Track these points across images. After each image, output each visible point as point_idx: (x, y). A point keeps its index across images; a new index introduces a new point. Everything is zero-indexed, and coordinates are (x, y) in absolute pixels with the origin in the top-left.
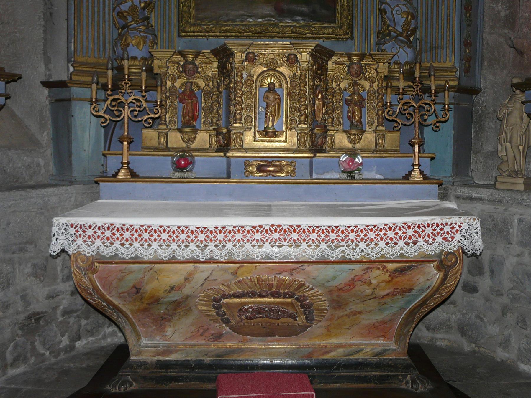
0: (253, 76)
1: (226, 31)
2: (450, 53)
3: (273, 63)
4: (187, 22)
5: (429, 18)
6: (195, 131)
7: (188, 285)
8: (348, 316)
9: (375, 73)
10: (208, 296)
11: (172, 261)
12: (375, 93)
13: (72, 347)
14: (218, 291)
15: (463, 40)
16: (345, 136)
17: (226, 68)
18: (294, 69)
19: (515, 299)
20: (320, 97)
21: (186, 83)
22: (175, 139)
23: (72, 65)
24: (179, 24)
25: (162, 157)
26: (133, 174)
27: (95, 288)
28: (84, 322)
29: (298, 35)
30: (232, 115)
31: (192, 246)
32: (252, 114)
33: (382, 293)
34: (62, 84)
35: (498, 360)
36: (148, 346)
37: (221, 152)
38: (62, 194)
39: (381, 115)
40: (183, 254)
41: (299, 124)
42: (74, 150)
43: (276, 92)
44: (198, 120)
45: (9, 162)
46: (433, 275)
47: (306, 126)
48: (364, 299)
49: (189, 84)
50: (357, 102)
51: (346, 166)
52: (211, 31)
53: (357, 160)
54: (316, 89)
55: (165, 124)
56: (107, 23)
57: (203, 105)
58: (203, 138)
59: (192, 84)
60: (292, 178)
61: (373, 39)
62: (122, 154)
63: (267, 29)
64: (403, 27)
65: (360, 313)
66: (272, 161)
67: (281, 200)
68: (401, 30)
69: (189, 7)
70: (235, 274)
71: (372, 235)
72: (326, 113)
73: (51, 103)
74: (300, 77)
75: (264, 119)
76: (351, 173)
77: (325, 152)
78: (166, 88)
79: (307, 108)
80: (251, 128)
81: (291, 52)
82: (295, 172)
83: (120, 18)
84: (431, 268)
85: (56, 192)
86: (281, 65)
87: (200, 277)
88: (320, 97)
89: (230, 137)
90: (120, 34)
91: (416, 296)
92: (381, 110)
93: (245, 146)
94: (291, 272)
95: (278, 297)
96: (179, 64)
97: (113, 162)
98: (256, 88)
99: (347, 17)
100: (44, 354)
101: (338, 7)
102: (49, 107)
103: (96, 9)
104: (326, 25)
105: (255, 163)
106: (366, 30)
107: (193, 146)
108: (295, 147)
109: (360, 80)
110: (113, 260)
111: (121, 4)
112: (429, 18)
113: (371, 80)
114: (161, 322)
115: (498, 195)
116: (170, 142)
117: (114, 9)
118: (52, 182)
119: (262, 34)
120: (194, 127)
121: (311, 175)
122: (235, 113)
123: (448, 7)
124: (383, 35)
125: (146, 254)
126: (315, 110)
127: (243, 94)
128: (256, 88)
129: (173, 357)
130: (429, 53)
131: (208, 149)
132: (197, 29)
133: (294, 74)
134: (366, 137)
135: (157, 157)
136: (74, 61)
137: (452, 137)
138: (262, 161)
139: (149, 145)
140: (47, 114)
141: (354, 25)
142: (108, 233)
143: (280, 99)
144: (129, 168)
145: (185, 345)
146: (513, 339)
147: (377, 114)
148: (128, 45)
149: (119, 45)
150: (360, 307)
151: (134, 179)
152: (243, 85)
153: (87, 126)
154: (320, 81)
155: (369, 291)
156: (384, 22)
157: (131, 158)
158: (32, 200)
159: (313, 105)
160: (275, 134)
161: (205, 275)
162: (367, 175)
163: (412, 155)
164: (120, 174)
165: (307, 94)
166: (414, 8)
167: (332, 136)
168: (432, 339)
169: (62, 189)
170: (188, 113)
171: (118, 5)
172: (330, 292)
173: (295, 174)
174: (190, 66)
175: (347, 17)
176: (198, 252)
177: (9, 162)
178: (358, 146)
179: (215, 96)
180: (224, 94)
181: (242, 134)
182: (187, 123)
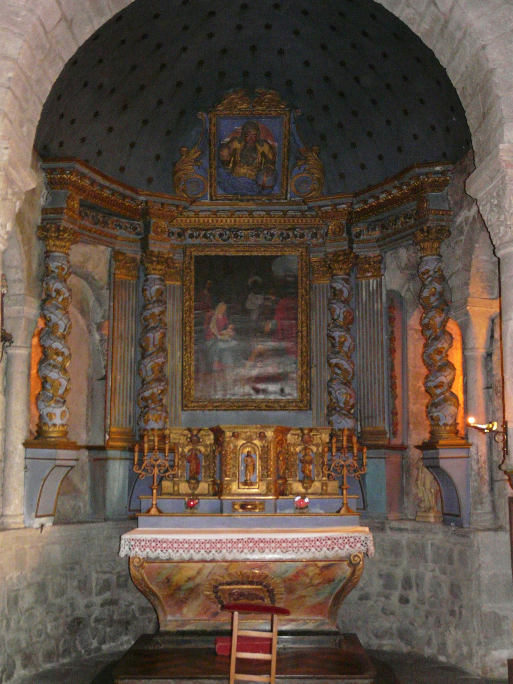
1: (217, 406)
6: (198, 482)
7: (199, 577)
8: (297, 599)
10: (210, 584)
11: (191, 561)
13: (99, 649)
14: (217, 580)
18: (264, 442)
19: (432, 605)
21: (192, 449)
22: (184, 488)
26: (160, 511)
27: (143, 579)
28: (108, 630)
31: (203, 552)
32: (237, 471)
33: (316, 582)
34: (102, 448)
35: (426, 656)
36: (171, 621)
40: (197, 557)
46: (346, 570)
48: (307, 586)
52: (205, 406)
58: (204, 487)
59: (196, 449)
61: (326, 411)
65: (304, 597)
70: (227, 569)
71: (307, 544)
75: (244, 474)
76: (302, 509)
77: (286, 495)
84: (345, 564)
86: (255, 439)
87: (206, 572)
89: (222, 486)
90: (142, 412)
91: (338, 584)
93: (163, 492)
94: (260, 568)
95: (253, 585)
100: (80, 652)
105: (239, 503)
107: (196, 492)
108: (264, 493)
110: (157, 559)
113: (317, 445)
114: (181, 603)
115: (417, 525)
118: (89, 520)
125: (175, 556)
129: (187, 628)
132: (196, 404)
140: (87, 469)
142: (154, 544)
144: (157, 507)
145: (195, 620)
146: (433, 638)
150: (304, 593)
155: (308, 581)
156: (331, 400)
157: (158, 501)
160: (251, 484)
161: (209, 570)
162: (313, 510)
167: (291, 484)
168: (380, 645)
172: (284, 581)
174: (195, 438)
175: (306, 395)
176: (206, 555)
178: (310, 491)
180: (218, 458)
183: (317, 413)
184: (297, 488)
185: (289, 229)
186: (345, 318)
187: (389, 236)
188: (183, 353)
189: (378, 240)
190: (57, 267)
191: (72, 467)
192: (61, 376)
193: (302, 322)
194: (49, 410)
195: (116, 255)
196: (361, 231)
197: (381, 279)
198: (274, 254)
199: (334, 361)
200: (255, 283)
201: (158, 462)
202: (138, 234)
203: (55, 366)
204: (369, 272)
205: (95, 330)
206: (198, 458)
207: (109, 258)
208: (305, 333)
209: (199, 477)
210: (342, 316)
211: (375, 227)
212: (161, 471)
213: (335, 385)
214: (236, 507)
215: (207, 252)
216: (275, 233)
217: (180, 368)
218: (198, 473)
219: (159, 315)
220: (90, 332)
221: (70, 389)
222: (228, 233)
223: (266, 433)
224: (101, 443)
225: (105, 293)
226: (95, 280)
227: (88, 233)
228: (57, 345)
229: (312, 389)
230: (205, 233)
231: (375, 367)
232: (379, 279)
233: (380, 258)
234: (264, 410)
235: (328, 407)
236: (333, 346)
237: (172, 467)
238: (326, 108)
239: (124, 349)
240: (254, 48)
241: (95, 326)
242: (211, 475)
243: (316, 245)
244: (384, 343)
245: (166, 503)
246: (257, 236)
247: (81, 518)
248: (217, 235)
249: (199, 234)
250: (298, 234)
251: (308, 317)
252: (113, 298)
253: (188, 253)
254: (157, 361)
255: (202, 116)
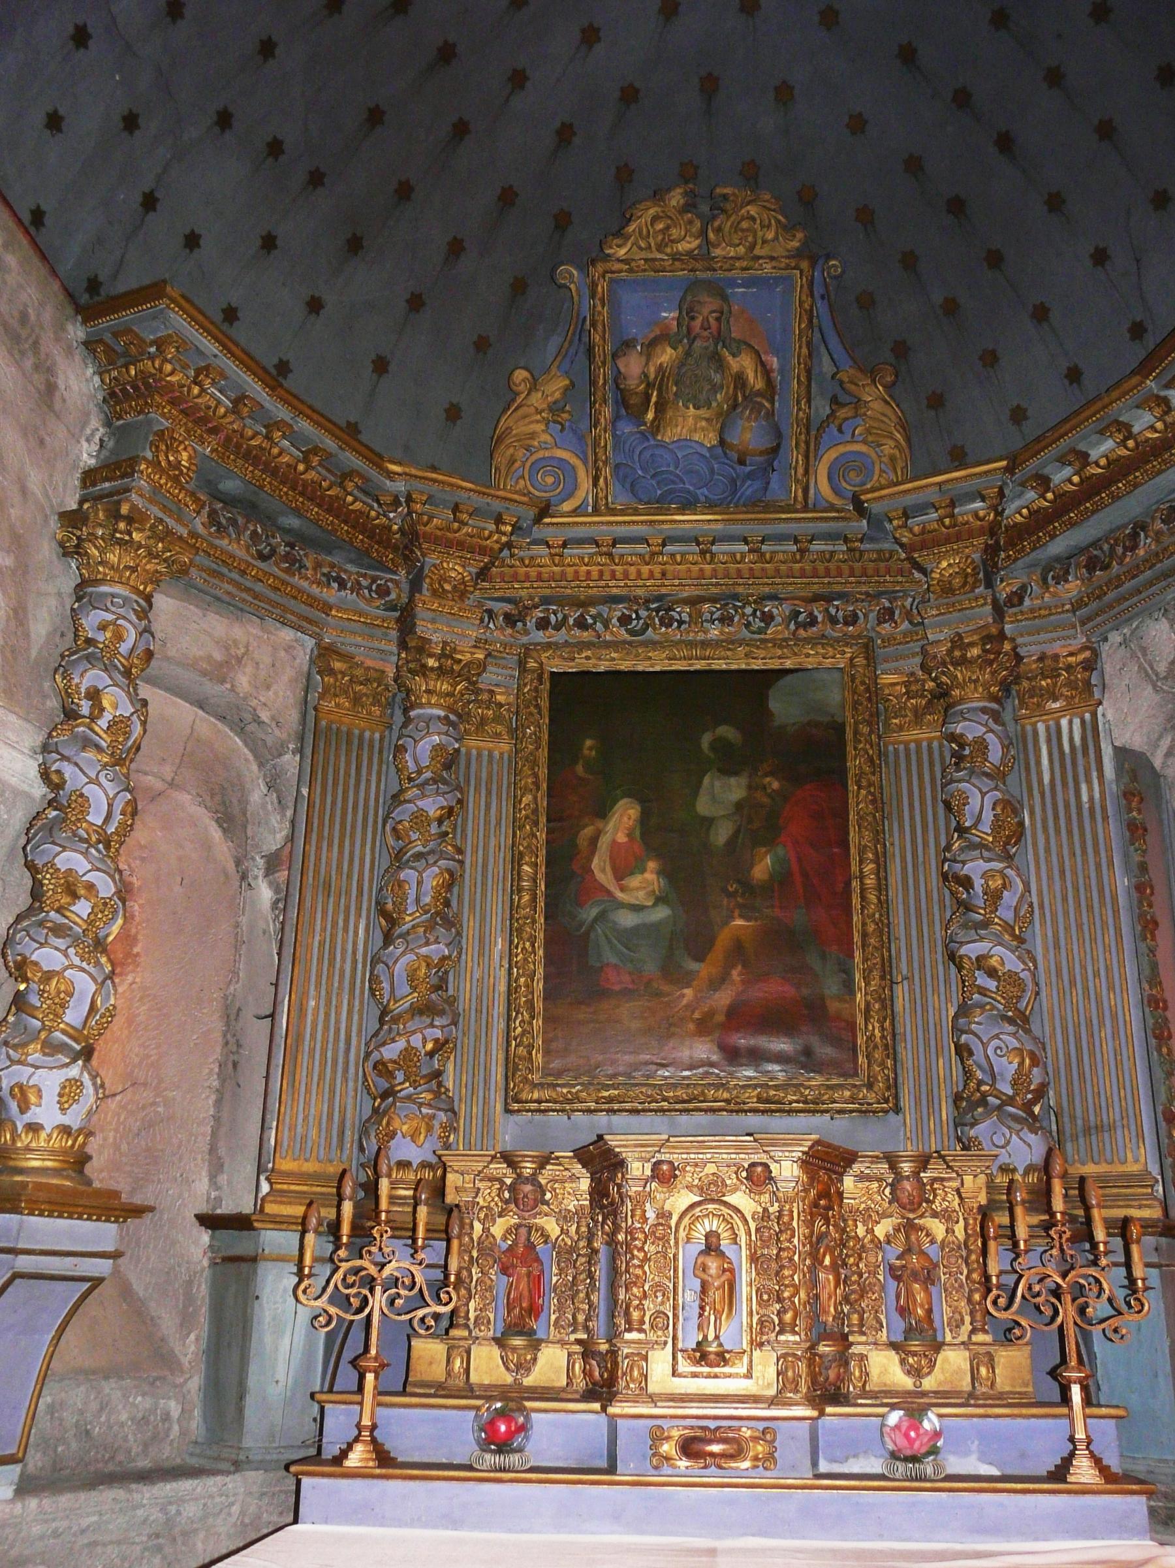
0: (671, 1214)
1: (610, 1100)
2: (1134, 1140)
3: (715, 1183)
4: (525, 1080)
5: (1074, 1059)
6: (535, 1345)
9: (957, 1200)
12: (959, 1248)
15: (1160, 1109)
16: (893, 1357)
17: (607, 1195)
18: (765, 1198)
20: (827, 1261)
21: (518, 1227)
22: (487, 1365)
23: (267, 1179)
24: (507, 1084)
25: (454, 1412)
29: (773, 1106)
30: (620, 1311)
34: (241, 1223)
37: (595, 1400)
38: (211, 1497)
39: (979, 1303)
41: (781, 1332)
42: (252, 1381)
43: (723, 1254)
44: (543, 1316)
45: (102, 1409)
47: (797, 1338)
49: (523, 1231)
50: (915, 1271)
51: (902, 1442)
53: (926, 1425)
54: (818, 1242)
55: (467, 1326)
56: (351, 1084)
57: (555, 1279)
58: (552, 1363)
59: (530, 1228)
60: (768, 1474)
61: (946, 1111)
62: (361, 1403)
63: (703, 1093)
64: (1015, 1083)
66: (718, 1428)
67: (745, 1534)
68: (1010, 1092)
69: (530, 1047)
72: (846, 1299)
73: (213, 1264)
74: (779, 1218)
75: (695, 1321)
76: (913, 1465)
78: (472, 1239)
79: (798, 1292)
80: (665, 1343)
81: (755, 1158)
82: (774, 1458)
83: (380, 1075)
85: (199, 1489)
86: (735, 1190)
88: (827, 1261)
89: (615, 1364)
90: (375, 1111)
92: (977, 1290)
96: (502, 1183)
97: (339, 1422)
98: (677, 1243)
99: (882, 1064)
101: (860, 1040)
102: (206, 1273)
103: (329, 1054)
104: (834, 1082)
105: (676, 1433)
106: (930, 1093)
108: (773, 1392)
109: (922, 1216)
111: (384, 1044)
112: (1074, 1059)
113: (946, 1216)
116: (476, 1370)
117: (368, 1055)
118: (194, 1462)
119: (691, 1106)
120: (531, 1333)
121: (815, 1464)
122: (628, 1307)
123: (1115, 1034)
124: (969, 1103)
126: (817, 1296)
127: (646, 1259)
128: (677, 1243)
130: (1081, 1140)
131: (563, 1390)
133: (765, 1210)
134: (946, 1360)
135: (443, 1412)
136: (273, 1170)
137: (1167, 1351)
138: (692, 1428)
139: (426, 1378)
140: (203, 1290)
141: (900, 1080)
143: (732, 1271)
144: (374, 1441)
147: (970, 1301)
148: (392, 1135)
149: (373, 1134)
151: (384, 1471)
152: (646, 1237)
153: (287, 1325)
154: (827, 1223)
156: (968, 1074)
157: (381, 1411)
158: (140, 1512)
159: (814, 1283)
160: (722, 1358)
162: (955, 1464)
163: (1065, 1410)
164: (351, 1455)
165: (796, 1258)
166: (1035, 1038)
167: (863, 1358)
169: (211, 1484)
170: (520, 1298)
171: (377, 1048)
173: (775, 1464)
174: (528, 1188)
175: (882, 1064)
177: (102, 1409)
178: (928, 1383)
179: (584, 1260)
180: (603, 1257)
181: (646, 1358)
182: (516, 1325)
183: (919, 1120)
184: (885, 1371)
185: (816, 598)
186: (997, 826)
187: (1117, 582)
188: (511, 942)
189: (1077, 605)
190: (103, 627)
191: (97, 1282)
192: (77, 961)
193: (862, 850)
194: (22, 1074)
195: (324, 654)
196: (1023, 588)
197: (1094, 715)
198: (774, 664)
199: (971, 951)
200: (720, 745)
201: (387, 1271)
202: (391, 607)
203: (58, 931)
204: (1055, 700)
205: (261, 873)
206: (538, 1260)
207: (305, 668)
208: (870, 881)
209: (539, 1326)
210: (988, 816)
211: (1067, 572)
212: (399, 1302)
213: (979, 1023)
214: (667, 1448)
215: (583, 662)
216: (775, 611)
217: (502, 987)
218: (534, 1310)
219: (440, 821)
220: (244, 877)
221: (111, 1013)
222: (643, 613)
223: (774, 1167)
224: (246, 1207)
225: (290, 762)
226: (260, 723)
227: (235, 575)
228: (72, 860)
229: (900, 1048)
230: (582, 615)
231: (1096, 974)
232: (1087, 716)
233: (1087, 654)
234: (755, 1111)
235: (957, 1098)
236: (967, 907)
237: (439, 1288)
238: (909, 261)
239: (335, 924)
240: (710, 85)
241: (261, 862)
242: (581, 1318)
243: (889, 640)
244: (1122, 901)
245: (414, 1428)
246: (726, 620)
247: (167, 1454)
248: (614, 621)
249: (565, 618)
250: (840, 613)
251: (878, 836)
252: (313, 773)
253: (532, 664)
254: (424, 950)
255: (569, 274)
